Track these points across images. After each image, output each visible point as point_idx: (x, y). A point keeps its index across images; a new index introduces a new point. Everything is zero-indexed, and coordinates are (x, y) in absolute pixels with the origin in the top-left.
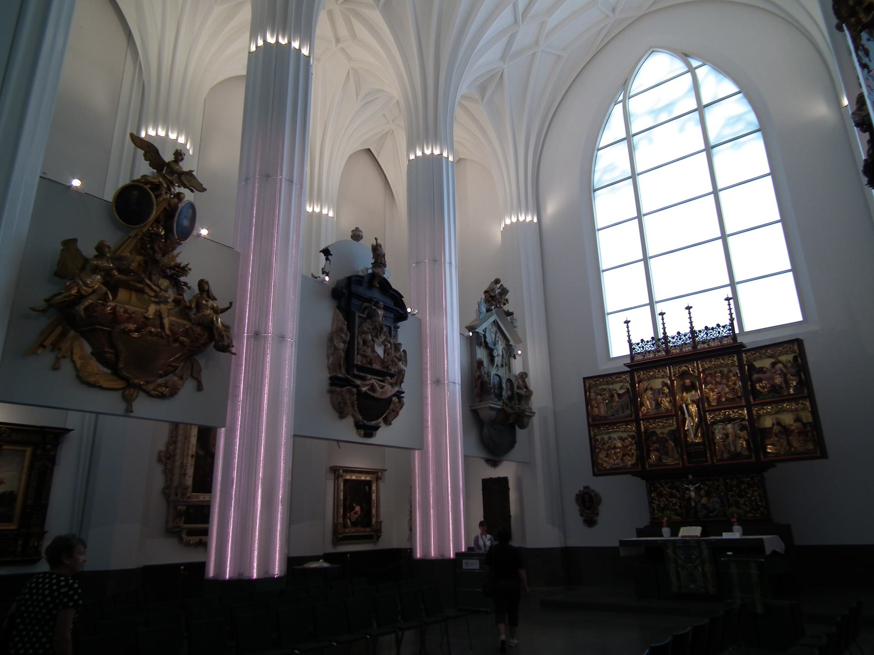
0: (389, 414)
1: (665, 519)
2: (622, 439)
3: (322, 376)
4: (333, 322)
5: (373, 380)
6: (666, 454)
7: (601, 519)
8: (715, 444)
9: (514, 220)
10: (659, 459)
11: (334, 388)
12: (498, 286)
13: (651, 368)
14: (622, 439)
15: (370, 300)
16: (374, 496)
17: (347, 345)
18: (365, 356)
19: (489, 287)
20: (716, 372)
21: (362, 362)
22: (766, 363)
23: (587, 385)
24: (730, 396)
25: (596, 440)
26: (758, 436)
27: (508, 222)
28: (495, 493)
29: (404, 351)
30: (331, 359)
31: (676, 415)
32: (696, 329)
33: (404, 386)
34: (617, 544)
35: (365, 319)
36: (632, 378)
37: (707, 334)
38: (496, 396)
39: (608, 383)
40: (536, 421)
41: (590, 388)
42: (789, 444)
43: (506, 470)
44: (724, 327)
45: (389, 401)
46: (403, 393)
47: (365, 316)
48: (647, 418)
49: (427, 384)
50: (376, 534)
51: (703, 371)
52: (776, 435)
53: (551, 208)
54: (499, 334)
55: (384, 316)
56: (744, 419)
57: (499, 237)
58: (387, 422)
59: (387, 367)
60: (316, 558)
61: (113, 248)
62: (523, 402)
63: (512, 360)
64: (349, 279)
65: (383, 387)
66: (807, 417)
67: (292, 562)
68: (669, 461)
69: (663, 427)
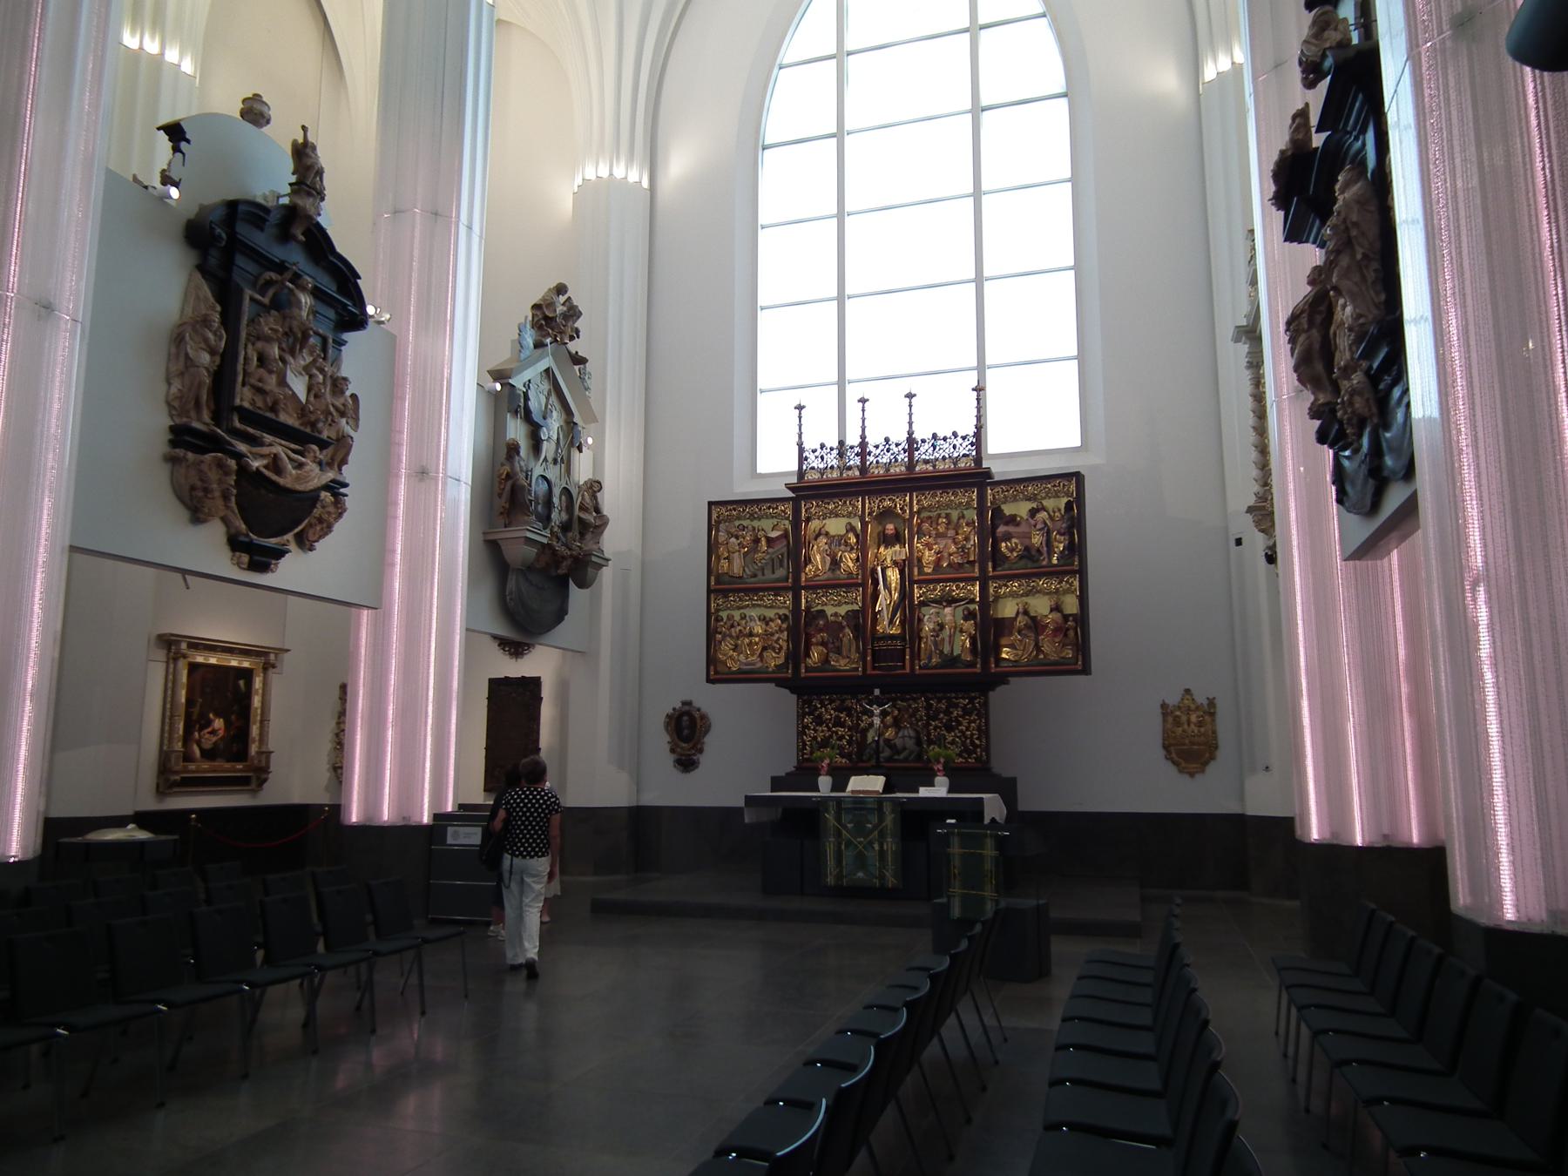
0: (310, 525)
1: (827, 761)
2: (765, 621)
3: (147, 422)
4: (185, 301)
5: (279, 448)
6: (839, 651)
7: (705, 760)
8: (920, 639)
9: (604, 172)
10: (826, 661)
11: (180, 452)
12: (562, 299)
13: (832, 496)
14: (765, 621)
15: (281, 267)
16: (256, 701)
17: (218, 360)
18: (260, 391)
19: (544, 299)
20: (939, 516)
21: (253, 403)
22: (1022, 509)
23: (714, 516)
24: (957, 559)
25: (718, 619)
26: (990, 630)
27: (590, 174)
28: (512, 707)
29: (354, 396)
30: (176, 386)
31: (864, 585)
32: (918, 436)
33: (348, 473)
34: (741, 803)
35: (267, 309)
36: (797, 511)
37: (934, 447)
38: (539, 518)
39: (752, 517)
40: (607, 574)
41: (718, 522)
42: (1038, 647)
43: (540, 663)
44: (964, 438)
45: (312, 498)
46: (346, 485)
47: (266, 300)
48: (812, 588)
49: (397, 476)
50: (258, 775)
51: (919, 512)
52: (1019, 632)
53: (679, 164)
54: (553, 399)
55: (314, 312)
56: (972, 601)
57: (567, 204)
58: (305, 543)
59: (313, 425)
60: (119, 822)
61: (298, 981)
62: (589, 536)
63: (575, 452)
64: (232, 206)
65: (300, 466)
66: (1071, 605)
67: (57, 832)
68: (841, 664)
69: (839, 604)
